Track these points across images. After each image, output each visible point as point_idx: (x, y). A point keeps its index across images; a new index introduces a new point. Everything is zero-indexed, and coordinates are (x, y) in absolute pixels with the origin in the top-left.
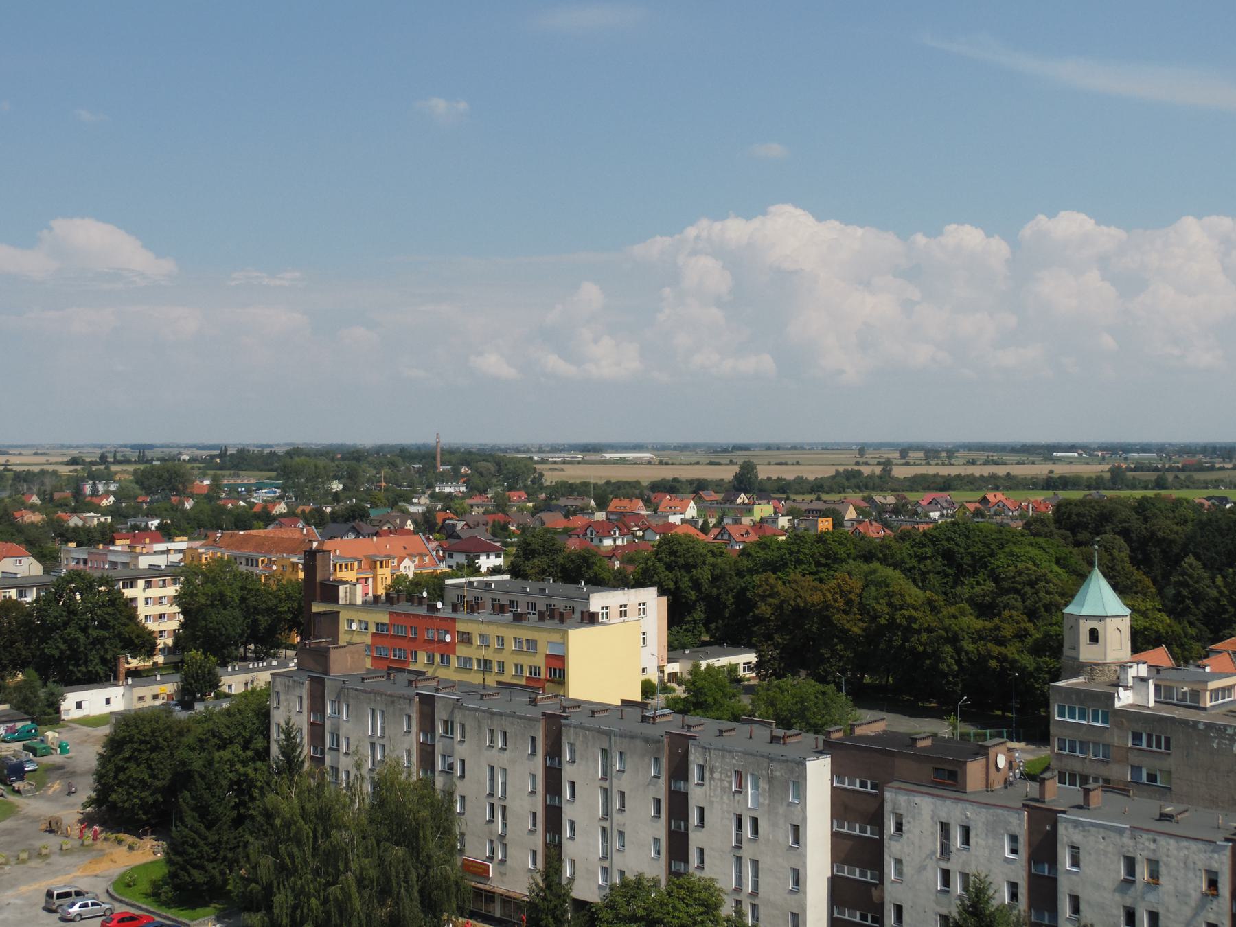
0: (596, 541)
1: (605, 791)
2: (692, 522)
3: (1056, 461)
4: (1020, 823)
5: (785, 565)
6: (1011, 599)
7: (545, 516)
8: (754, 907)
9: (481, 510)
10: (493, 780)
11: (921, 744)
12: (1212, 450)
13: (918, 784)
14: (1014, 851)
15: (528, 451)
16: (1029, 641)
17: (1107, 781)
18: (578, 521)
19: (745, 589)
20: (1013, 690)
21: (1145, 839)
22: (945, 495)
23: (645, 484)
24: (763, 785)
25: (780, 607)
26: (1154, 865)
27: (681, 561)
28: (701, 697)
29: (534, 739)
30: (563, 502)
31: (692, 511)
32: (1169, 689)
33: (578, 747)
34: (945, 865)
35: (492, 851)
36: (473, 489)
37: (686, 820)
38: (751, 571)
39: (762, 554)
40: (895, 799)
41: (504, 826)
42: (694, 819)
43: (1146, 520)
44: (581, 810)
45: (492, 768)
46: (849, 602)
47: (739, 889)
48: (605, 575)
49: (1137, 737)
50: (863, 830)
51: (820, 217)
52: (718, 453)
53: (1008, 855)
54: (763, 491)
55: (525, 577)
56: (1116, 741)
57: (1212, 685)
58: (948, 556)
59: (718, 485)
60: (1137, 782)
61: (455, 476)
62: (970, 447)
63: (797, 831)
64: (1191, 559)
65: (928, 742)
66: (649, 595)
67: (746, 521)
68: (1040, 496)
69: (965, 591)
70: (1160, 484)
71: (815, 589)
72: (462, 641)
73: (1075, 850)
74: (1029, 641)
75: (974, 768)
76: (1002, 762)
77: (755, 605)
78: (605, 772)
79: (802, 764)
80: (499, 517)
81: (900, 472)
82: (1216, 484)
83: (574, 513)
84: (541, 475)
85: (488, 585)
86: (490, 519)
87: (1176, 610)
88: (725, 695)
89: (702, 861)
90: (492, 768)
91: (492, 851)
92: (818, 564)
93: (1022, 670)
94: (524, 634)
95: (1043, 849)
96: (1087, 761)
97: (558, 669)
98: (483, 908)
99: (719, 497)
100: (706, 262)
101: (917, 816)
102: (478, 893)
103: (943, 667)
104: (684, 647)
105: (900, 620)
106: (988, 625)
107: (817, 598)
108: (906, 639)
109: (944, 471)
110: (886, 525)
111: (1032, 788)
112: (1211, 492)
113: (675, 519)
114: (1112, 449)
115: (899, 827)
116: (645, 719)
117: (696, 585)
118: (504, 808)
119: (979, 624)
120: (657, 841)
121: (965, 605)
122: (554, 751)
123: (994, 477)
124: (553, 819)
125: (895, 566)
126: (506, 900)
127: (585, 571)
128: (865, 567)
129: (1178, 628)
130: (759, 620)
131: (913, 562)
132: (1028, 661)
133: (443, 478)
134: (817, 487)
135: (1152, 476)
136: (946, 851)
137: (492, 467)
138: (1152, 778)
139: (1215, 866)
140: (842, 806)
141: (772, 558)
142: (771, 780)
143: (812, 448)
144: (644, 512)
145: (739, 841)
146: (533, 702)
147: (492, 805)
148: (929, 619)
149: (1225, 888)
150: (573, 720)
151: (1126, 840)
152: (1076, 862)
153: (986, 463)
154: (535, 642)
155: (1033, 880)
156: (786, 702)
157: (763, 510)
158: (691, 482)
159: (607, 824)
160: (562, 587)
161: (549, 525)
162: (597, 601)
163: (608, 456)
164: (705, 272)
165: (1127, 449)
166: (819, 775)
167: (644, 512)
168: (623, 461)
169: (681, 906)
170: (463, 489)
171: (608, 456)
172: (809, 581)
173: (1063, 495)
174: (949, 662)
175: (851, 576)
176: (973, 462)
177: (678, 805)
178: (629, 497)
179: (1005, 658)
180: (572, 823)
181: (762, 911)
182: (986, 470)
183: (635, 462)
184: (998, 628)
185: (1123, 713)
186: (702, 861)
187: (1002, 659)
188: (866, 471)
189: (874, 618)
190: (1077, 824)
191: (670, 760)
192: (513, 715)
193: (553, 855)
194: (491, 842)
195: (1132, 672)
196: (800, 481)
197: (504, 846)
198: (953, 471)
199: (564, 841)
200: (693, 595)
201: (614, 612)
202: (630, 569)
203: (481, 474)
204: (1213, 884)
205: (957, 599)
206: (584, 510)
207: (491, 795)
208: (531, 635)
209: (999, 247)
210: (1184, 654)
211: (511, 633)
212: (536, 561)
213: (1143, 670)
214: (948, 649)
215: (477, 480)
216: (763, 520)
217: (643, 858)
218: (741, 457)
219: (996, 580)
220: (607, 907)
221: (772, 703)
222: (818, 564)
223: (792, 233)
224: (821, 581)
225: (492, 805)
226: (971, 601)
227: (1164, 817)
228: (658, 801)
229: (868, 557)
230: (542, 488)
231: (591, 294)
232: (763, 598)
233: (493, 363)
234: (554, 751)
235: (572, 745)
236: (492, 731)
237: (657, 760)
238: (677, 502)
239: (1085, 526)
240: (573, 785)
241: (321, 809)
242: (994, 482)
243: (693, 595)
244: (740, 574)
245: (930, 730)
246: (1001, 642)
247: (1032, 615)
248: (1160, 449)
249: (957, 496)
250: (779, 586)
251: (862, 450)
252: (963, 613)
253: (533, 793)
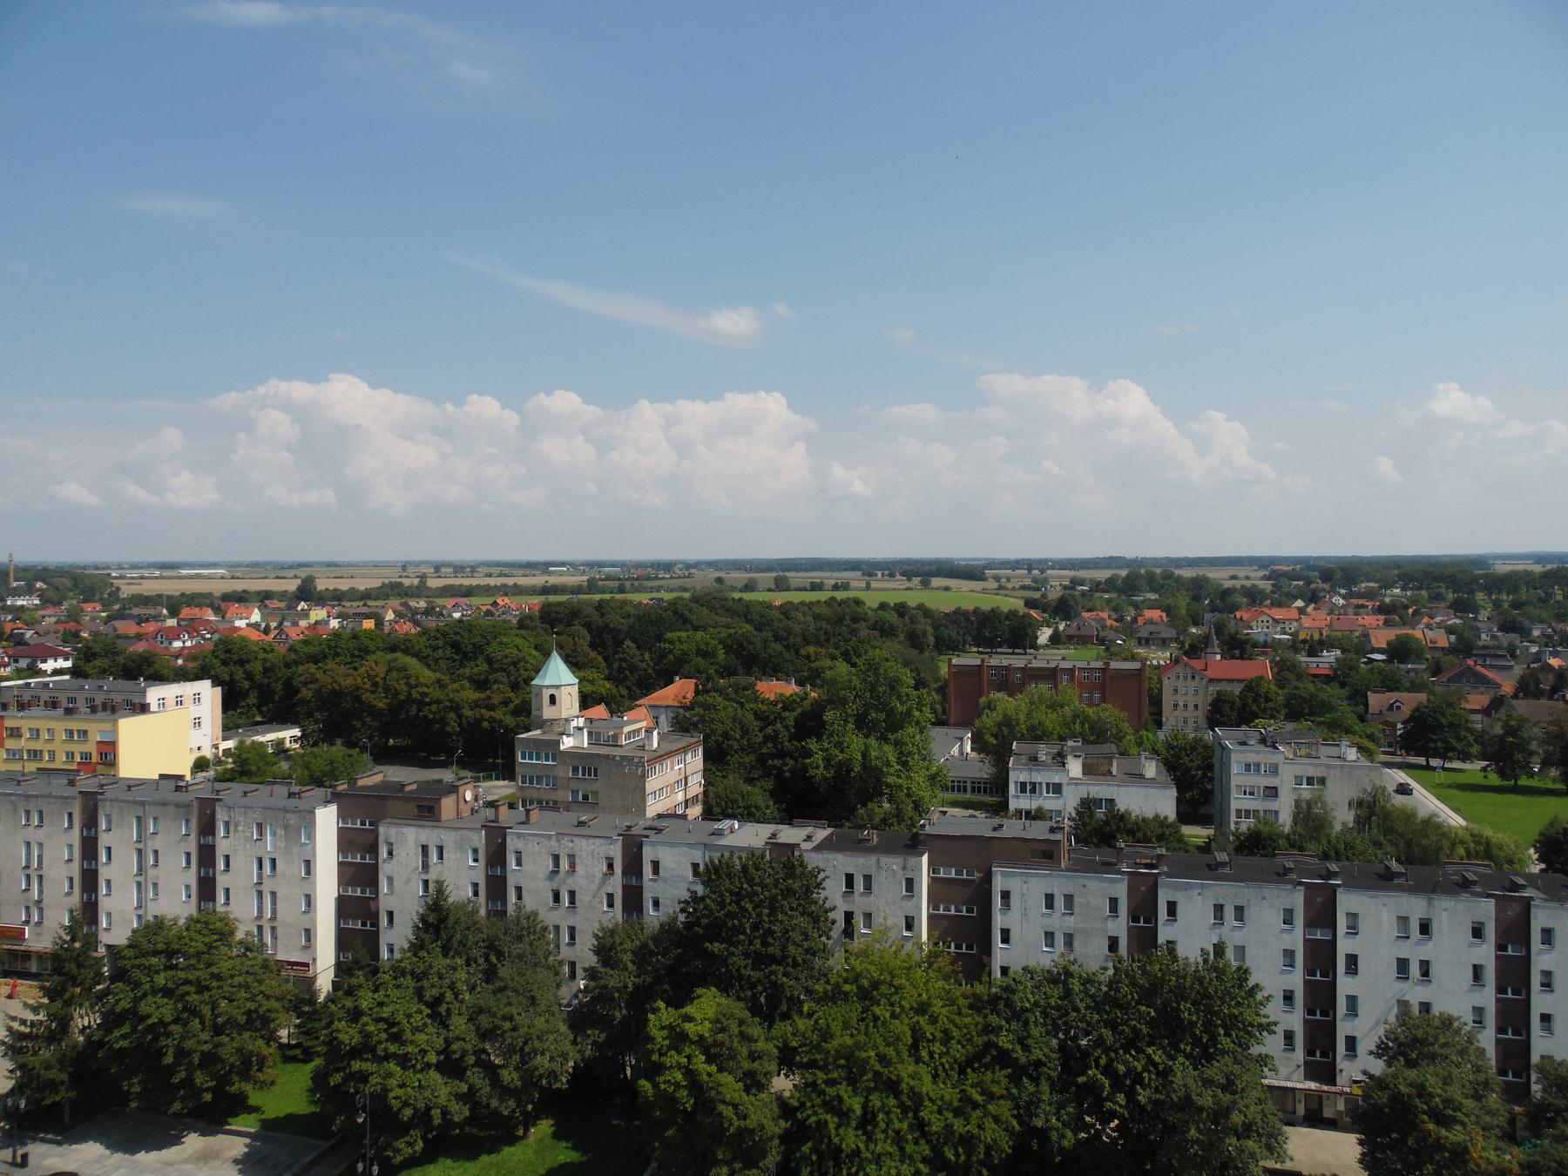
0: (166, 644)
1: (140, 851)
2: (255, 626)
3: (550, 574)
4: (479, 839)
5: (325, 657)
6: (500, 676)
7: (116, 623)
8: (273, 929)
9: (54, 619)
10: (29, 854)
11: (407, 789)
12: (657, 565)
13: (404, 819)
14: (476, 860)
15: (108, 568)
16: (511, 706)
17: (540, 802)
18: (150, 627)
19: (291, 678)
20: (490, 742)
21: (566, 842)
22: (466, 600)
23: (217, 595)
24: (280, 832)
25: (319, 691)
26: (572, 857)
27: (235, 658)
28: (245, 768)
29: (70, 815)
30: (136, 611)
31: (256, 616)
32: (598, 734)
33: (114, 818)
34: (425, 877)
35: (28, 915)
36: (46, 602)
37: (214, 866)
38: (297, 663)
39: (306, 650)
40: (386, 831)
41: (41, 892)
42: (221, 865)
43: (602, 615)
44: (118, 871)
45: (28, 844)
46: (375, 684)
47: (260, 917)
48: (165, 672)
49: (575, 770)
50: (363, 858)
51: (374, 387)
52: (281, 569)
53: (471, 863)
54: (319, 599)
55: (86, 676)
56: (561, 774)
57: (626, 730)
58: (456, 646)
59: (282, 595)
60: (575, 802)
61: (29, 590)
62: (488, 564)
63: (309, 865)
64: (628, 642)
65: (414, 787)
66: (205, 687)
67: (303, 623)
68: (537, 600)
69: (467, 671)
70: (621, 590)
71: (348, 675)
72: (11, 735)
73: (518, 853)
74: (511, 706)
75: (447, 804)
76: (469, 796)
77: (298, 691)
78: (139, 836)
79: (312, 812)
80: (72, 626)
81: (433, 583)
82: (658, 589)
83: (147, 620)
84: (118, 589)
85: (46, 685)
86: (61, 627)
87: (617, 678)
88: (267, 764)
89: (228, 898)
90: (28, 844)
91: (28, 915)
92: (353, 656)
93: (506, 728)
94: (75, 725)
95: (496, 857)
96: (542, 790)
97: (108, 752)
98: (19, 966)
99: (282, 605)
100: (277, 415)
101: (403, 845)
102: (13, 954)
103: (449, 729)
104: (238, 727)
105: (415, 695)
106: (482, 696)
107: (349, 682)
108: (419, 710)
109: (467, 582)
110: (416, 623)
111: (490, 813)
112: (655, 595)
113: (238, 623)
114: (591, 565)
115: (390, 853)
116: (178, 789)
117: (249, 676)
118: (41, 877)
119: (475, 695)
120: (188, 887)
121: (466, 683)
122: (90, 822)
123: (504, 586)
124: (90, 880)
125: (416, 655)
126: (41, 956)
127: (151, 669)
128: (389, 657)
129: (615, 691)
130: (303, 702)
131: (429, 651)
132: (510, 721)
133: (17, 593)
134: (366, 596)
135: (616, 584)
136: (425, 866)
137: (68, 583)
138: (585, 797)
139: (612, 854)
140: (346, 841)
141: (321, 650)
142: (286, 827)
143: (365, 565)
144: (213, 618)
145: (260, 876)
146: (72, 783)
147: (28, 876)
148: (437, 694)
149: (618, 869)
150: (108, 795)
151: (553, 843)
152: (519, 863)
153: (500, 575)
154: (85, 732)
155: (490, 879)
156: (319, 764)
157: (318, 614)
158: (258, 593)
159: (141, 879)
160: (123, 684)
161: (121, 631)
162: (154, 694)
163: (184, 572)
164: (276, 422)
165: (601, 565)
166: (327, 820)
167: (213, 618)
168: (198, 576)
169: (198, 937)
170: (37, 602)
171: (184, 572)
172: (343, 670)
173: (552, 598)
174: (453, 726)
175: (377, 664)
176: (490, 575)
177: (206, 856)
178: (200, 606)
179: (494, 720)
180: (108, 882)
181: (280, 932)
182: (499, 581)
183: (209, 577)
184: (489, 698)
185: (566, 753)
186: (228, 898)
187: (492, 720)
188: (407, 582)
189: (396, 694)
190: (519, 836)
191: (200, 820)
192: (50, 796)
193: (90, 910)
194: (27, 908)
195: (574, 724)
196: (352, 590)
197: (41, 910)
198: (474, 582)
199: (1339, 1017)
200: (246, 685)
201: (171, 702)
202: (191, 665)
203: (57, 589)
204: (610, 866)
205: (462, 677)
206: (156, 618)
207: (27, 867)
208: (82, 726)
209: (511, 419)
210: (617, 707)
211: (61, 726)
212: (98, 663)
213: (581, 722)
214: (452, 715)
215: (52, 594)
216: (317, 623)
217: (175, 901)
218: (303, 573)
219: (490, 662)
220: (130, 946)
221: (307, 766)
222: (353, 656)
223: (349, 396)
224: (355, 669)
225: (28, 876)
226: (471, 679)
227: (581, 824)
228: (188, 855)
229: (393, 649)
230: (118, 600)
231: (172, 437)
232: (305, 684)
233: (73, 491)
234: (90, 822)
235: (108, 817)
236: (28, 812)
237: (187, 821)
238: (242, 610)
239: (560, 621)
240: (109, 849)
241: (1219, 949)
242: (504, 590)
243: (246, 685)
244: (288, 666)
245: (407, 776)
246: (491, 708)
247: (515, 687)
248: (623, 565)
249: (475, 601)
250: (319, 675)
251: (404, 567)
252: (463, 688)
253: (70, 860)
